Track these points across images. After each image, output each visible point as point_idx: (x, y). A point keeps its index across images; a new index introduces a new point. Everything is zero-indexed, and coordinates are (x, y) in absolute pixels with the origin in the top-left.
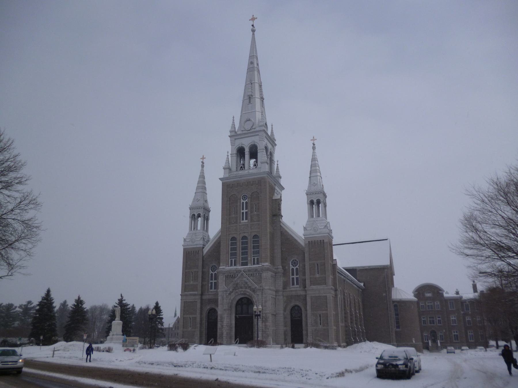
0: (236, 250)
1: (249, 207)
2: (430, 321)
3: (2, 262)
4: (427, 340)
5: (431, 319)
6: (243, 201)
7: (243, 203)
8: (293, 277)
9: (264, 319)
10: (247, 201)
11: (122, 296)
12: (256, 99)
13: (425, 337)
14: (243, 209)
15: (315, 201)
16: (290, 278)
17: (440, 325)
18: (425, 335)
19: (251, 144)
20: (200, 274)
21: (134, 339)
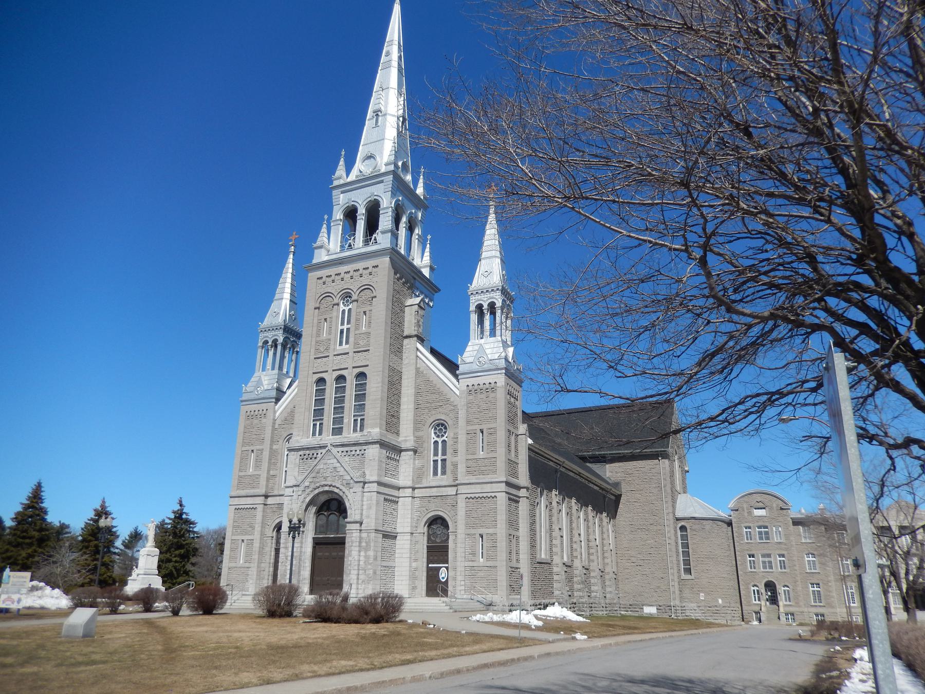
0: (343, 413)
1: (353, 320)
2: (764, 562)
3: (871, 596)
4: (759, 600)
5: (767, 559)
6: (344, 308)
7: (344, 311)
8: (436, 458)
9: (364, 544)
10: (350, 307)
11: (181, 505)
12: (388, 117)
13: (754, 594)
14: (342, 324)
15: (485, 306)
16: (428, 461)
17: (784, 570)
18: (754, 591)
19: (370, 199)
20: (266, 454)
21: (23, 577)
